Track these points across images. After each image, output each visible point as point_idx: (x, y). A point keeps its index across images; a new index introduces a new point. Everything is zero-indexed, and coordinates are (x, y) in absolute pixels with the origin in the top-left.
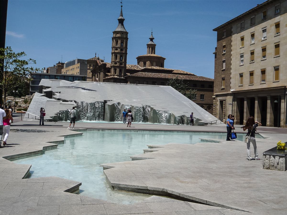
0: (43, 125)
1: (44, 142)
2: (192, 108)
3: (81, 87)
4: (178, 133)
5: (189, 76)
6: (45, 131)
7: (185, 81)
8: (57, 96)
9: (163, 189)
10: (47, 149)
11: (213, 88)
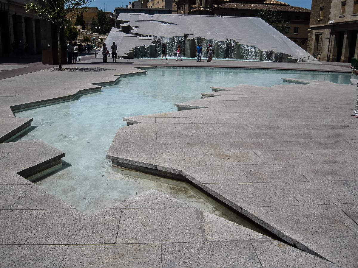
0: (106, 62)
1: (88, 84)
2: (282, 42)
3: (162, 20)
4: (260, 71)
5: (283, 7)
6: (104, 70)
7: (278, 12)
8: (135, 30)
9: (181, 171)
10: (86, 93)
11: (309, 20)
